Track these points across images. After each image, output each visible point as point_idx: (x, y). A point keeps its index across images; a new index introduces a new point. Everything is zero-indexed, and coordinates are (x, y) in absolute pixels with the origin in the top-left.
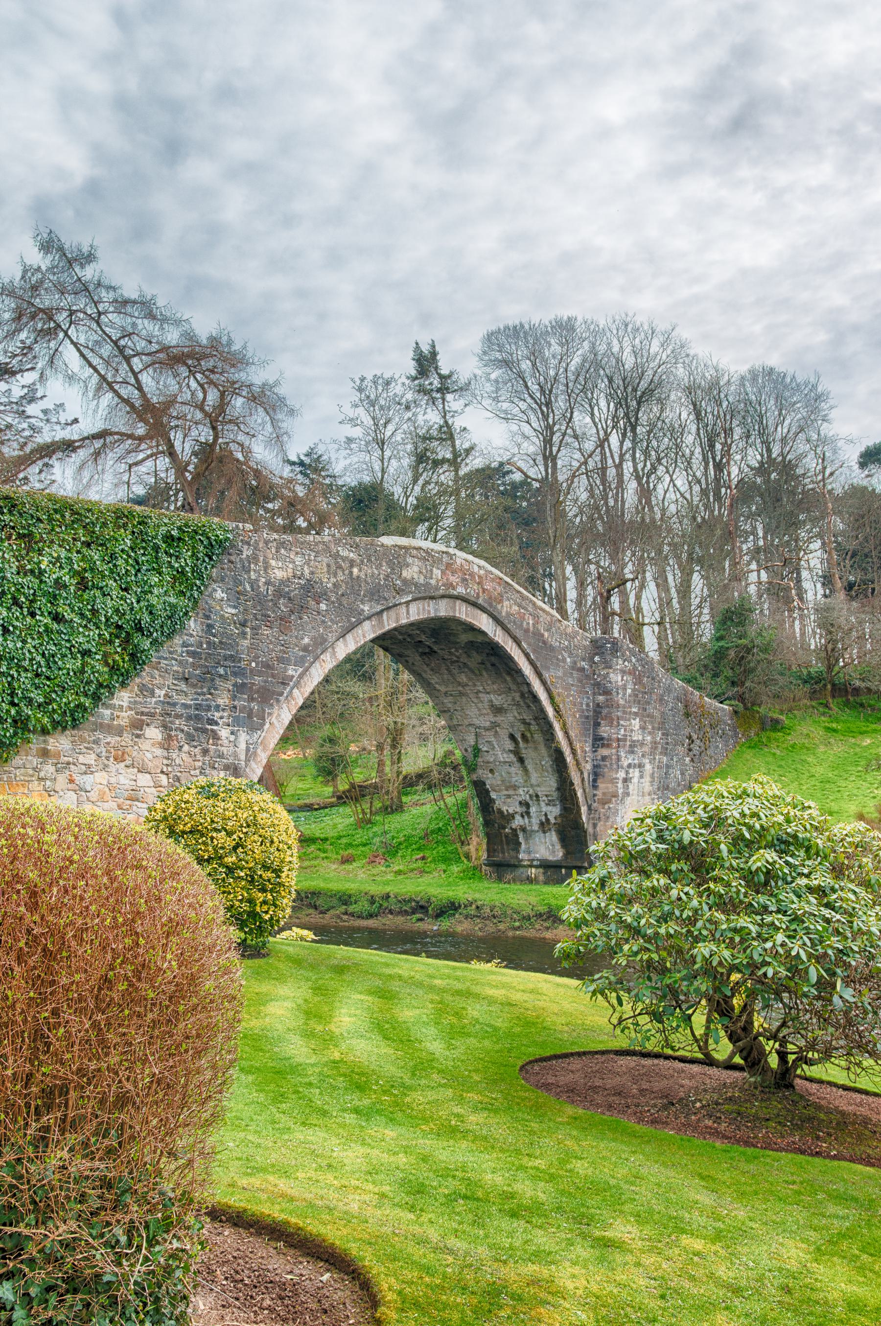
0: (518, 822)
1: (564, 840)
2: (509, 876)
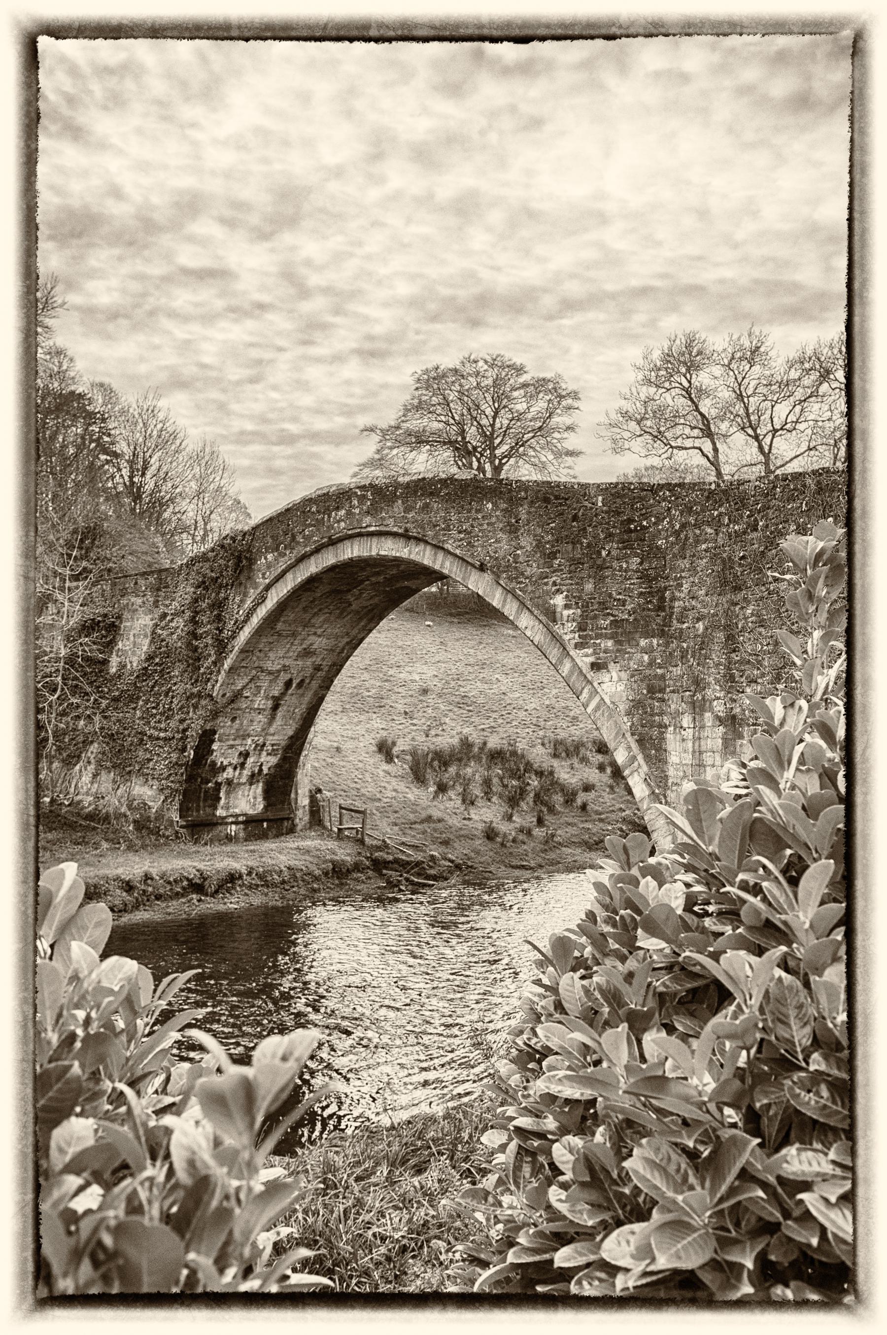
0: (229, 773)
1: (268, 794)
2: (206, 837)
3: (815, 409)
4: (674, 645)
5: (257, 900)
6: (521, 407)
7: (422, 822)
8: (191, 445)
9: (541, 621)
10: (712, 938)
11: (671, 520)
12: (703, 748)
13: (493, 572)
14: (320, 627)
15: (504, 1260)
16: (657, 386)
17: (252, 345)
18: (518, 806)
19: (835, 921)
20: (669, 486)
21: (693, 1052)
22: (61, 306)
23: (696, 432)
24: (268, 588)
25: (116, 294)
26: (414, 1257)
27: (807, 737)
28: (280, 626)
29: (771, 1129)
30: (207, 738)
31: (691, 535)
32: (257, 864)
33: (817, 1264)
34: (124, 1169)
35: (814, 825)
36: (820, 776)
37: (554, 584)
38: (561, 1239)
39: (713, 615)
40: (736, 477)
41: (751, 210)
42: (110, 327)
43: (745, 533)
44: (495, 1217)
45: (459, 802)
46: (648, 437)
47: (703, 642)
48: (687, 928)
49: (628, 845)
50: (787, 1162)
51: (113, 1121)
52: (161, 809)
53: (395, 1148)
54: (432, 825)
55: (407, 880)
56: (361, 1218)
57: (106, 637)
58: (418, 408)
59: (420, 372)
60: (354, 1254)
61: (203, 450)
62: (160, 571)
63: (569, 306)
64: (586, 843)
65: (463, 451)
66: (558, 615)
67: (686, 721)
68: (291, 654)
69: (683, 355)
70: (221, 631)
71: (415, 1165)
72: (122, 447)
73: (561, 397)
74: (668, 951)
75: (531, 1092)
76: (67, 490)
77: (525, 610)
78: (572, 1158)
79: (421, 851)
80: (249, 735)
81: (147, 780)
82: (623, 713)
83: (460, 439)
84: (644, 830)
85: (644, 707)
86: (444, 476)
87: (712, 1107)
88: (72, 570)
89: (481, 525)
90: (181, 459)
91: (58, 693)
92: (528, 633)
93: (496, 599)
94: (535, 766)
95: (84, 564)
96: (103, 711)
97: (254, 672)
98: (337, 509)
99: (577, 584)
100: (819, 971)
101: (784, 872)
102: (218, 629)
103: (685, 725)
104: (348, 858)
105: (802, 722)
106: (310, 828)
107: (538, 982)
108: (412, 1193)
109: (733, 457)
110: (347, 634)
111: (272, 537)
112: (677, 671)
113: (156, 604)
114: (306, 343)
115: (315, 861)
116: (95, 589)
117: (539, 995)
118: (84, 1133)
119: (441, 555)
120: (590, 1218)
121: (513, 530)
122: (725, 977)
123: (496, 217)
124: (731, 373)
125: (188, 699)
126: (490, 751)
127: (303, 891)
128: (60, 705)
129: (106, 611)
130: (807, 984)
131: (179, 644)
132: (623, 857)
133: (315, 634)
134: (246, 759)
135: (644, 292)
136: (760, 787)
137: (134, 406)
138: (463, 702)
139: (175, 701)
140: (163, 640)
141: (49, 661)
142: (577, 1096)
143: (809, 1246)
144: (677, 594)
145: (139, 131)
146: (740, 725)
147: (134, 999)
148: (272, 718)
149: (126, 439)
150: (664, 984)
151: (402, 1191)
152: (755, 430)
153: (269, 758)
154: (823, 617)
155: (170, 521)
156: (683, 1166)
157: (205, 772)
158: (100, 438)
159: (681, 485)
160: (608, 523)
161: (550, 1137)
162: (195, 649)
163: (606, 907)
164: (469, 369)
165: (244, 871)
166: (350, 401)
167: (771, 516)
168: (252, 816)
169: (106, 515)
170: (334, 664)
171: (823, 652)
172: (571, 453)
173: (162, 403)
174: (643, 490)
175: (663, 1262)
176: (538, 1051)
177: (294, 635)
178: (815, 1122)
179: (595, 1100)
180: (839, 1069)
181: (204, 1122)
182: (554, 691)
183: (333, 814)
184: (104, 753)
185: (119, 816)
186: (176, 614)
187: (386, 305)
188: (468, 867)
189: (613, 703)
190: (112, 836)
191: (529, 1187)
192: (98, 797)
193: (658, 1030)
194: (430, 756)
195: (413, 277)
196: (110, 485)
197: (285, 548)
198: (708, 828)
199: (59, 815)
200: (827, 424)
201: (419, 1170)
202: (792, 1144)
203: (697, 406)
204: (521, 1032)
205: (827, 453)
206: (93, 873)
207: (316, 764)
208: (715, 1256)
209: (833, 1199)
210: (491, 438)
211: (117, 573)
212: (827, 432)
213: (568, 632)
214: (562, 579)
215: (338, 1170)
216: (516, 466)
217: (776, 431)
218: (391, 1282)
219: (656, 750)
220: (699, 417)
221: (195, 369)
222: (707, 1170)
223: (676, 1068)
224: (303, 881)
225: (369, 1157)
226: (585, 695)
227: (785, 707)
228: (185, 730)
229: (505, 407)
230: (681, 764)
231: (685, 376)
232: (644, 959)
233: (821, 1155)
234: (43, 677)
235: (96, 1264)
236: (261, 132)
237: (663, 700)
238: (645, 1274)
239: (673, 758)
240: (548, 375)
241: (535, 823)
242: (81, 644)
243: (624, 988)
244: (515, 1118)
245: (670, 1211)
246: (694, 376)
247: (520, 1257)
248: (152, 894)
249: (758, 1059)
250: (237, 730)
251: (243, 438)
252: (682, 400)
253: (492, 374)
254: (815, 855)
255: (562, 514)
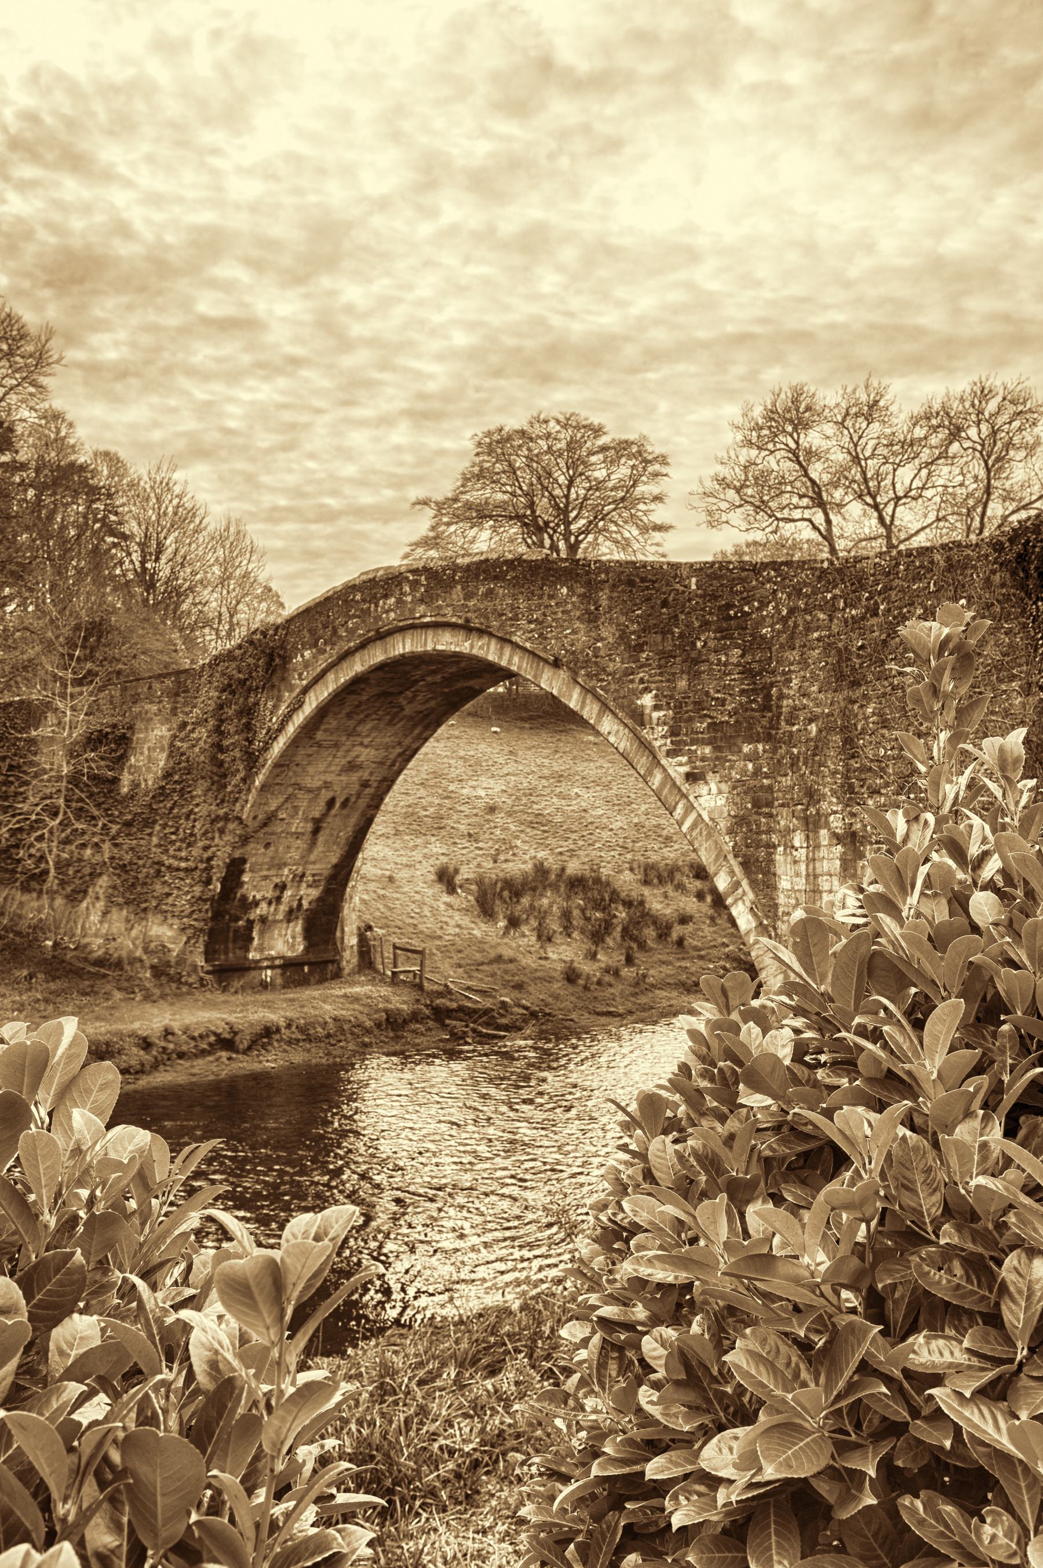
0: (263, 909)
1: (309, 933)
2: (237, 984)
3: (944, 473)
4: (782, 751)
5: (298, 1057)
6: (600, 474)
7: (491, 962)
8: (213, 523)
9: (626, 725)
10: (825, 1092)
11: (777, 605)
12: (819, 871)
13: (569, 669)
14: (368, 736)
15: (588, 1473)
16: (759, 448)
17: (285, 406)
18: (603, 941)
19: (968, 1070)
20: (774, 565)
21: (803, 1226)
22: (58, 362)
23: (805, 501)
24: (305, 690)
25: (124, 349)
26: (487, 1473)
27: (935, 856)
28: (320, 735)
29: (898, 1315)
30: (235, 868)
31: (800, 621)
32: (297, 1015)
33: (952, 1469)
34: (135, 1375)
35: (942, 958)
36: (949, 902)
37: (642, 681)
38: (654, 1447)
39: (828, 715)
40: (853, 554)
41: (866, 244)
42: (119, 387)
43: (863, 618)
44: (578, 1423)
45: (534, 939)
46: (749, 507)
47: (816, 747)
48: (796, 1081)
49: (727, 985)
50: (915, 1352)
51: (123, 1319)
52: (183, 952)
53: (464, 1345)
54: (502, 966)
55: (474, 1031)
56: (425, 1428)
57: (115, 751)
58: (479, 476)
59: (481, 435)
60: (418, 1471)
61: (227, 529)
62: (179, 673)
63: (654, 357)
64: (683, 984)
65: (534, 527)
66: (646, 718)
67: (798, 839)
68: (333, 768)
69: (789, 411)
70: (251, 743)
71: (488, 1366)
72: (132, 527)
73: (647, 462)
74: (774, 1108)
75: (618, 1277)
76: (67, 578)
77: (607, 712)
78: (666, 1352)
79: (490, 996)
80: (285, 865)
81: (166, 918)
82: (724, 831)
83: (528, 512)
84: (753, 971)
85: (749, 824)
86: (510, 556)
87: (827, 1289)
88: (74, 673)
89: (555, 613)
90: (201, 540)
91: (60, 817)
92: (612, 739)
93: (573, 702)
94: (623, 895)
95: (89, 665)
96: (113, 838)
97: (290, 790)
98: (386, 597)
99: (668, 681)
100: (949, 1129)
101: (908, 1014)
102: (247, 739)
103: (797, 844)
104: (405, 1007)
105: (928, 838)
106: (359, 972)
107: (624, 1148)
108: (484, 1398)
109: (849, 529)
110: (400, 744)
111: (309, 631)
112: (787, 781)
113: (174, 712)
114: (347, 403)
115: (366, 1010)
116: (101, 695)
117: (626, 1163)
118: (89, 1332)
119: (507, 650)
120: (686, 1422)
121: (592, 619)
122: (840, 1137)
123: (568, 254)
124: (846, 432)
125: (213, 822)
126: (570, 878)
127: (351, 1046)
128: (63, 831)
129: (115, 720)
130: (936, 1145)
131: (202, 758)
132: (721, 1000)
133: (361, 744)
134: (282, 892)
135: (742, 339)
136: (880, 915)
137: (146, 478)
138: (538, 821)
139: (198, 825)
140: (183, 754)
141: (49, 781)
142: (670, 1279)
143: (942, 1448)
144: (785, 691)
145: (150, 159)
146: (862, 844)
147: (147, 1173)
148: (313, 843)
149: (137, 519)
150: (770, 1147)
151: (473, 1396)
152: (874, 498)
153: (310, 891)
154: (950, 716)
155: (189, 613)
156: (794, 1359)
157: (233, 907)
158: (105, 517)
159: (788, 563)
160: (703, 609)
161: (639, 1328)
162: (221, 764)
163: (702, 1059)
164: (538, 430)
165: (282, 1023)
166: (400, 471)
167: (893, 598)
168: (290, 959)
169: (114, 606)
170: (384, 779)
171: (951, 757)
172: (659, 528)
173: (177, 476)
174: (743, 569)
175: (770, 1472)
176: (625, 1229)
177: (336, 745)
178: (948, 1304)
179: (691, 1284)
180: (974, 1241)
181: (228, 1316)
182: (643, 807)
183: (386, 954)
184: (114, 887)
185: (133, 961)
186: (197, 724)
187: (440, 357)
188: (546, 1014)
189: (712, 819)
190: (125, 984)
191: (616, 1388)
192: (110, 939)
193: (764, 1202)
194: (499, 885)
195: (471, 326)
196: (118, 572)
197: (325, 643)
198: (819, 964)
199: (63, 961)
200: (959, 490)
201: (493, 1371)
202: (919, 1332)
203: (806, 471)
204: (605, 1207)
205: (959, 525)
206: (101, 1029)
207: (366, 897)
208: (831, 1462)
209: (968, 1395)
210: (566, 512)
211: (128, 676)
212: (959, 500)
213: (658, 737)
214: (650, 676)
215: (398, 1373)
216: (595, 544)
217: (898, 498)
218: (461, 1503)
219: (764, 874)
220: (809, 484)
221: (217, 435)
222: (822, 1364)
223: (785, 1245)
224: (352, 1034)
225: (434, 1357)
226: (679, 811)
227: (908, 822)
228: (210, 859)
229: (581, 474)
230: (792, 890)
231: (791, 436)
232: (747, 1118)
233: (954, 1343)
234: (43, 799)
235: (102, 1485)
236: (293, 158)
237: (770, 815)
238: (751, 1486)
239: (784, 884)
240: (632, 437)
241: (623, 962)
242: (87, 760)
243: (722, 1152)
244: (599, 1307)
245: (779, 1412)
246: (802, 436)
247: (606, 1469)
248: (173, 1051)
249: (880, 1232)
250: (272, 858)
251: (274, 516)
252: (789, 464)
253: (565, 435)
254: (944, 994)
255: (649, 599)
